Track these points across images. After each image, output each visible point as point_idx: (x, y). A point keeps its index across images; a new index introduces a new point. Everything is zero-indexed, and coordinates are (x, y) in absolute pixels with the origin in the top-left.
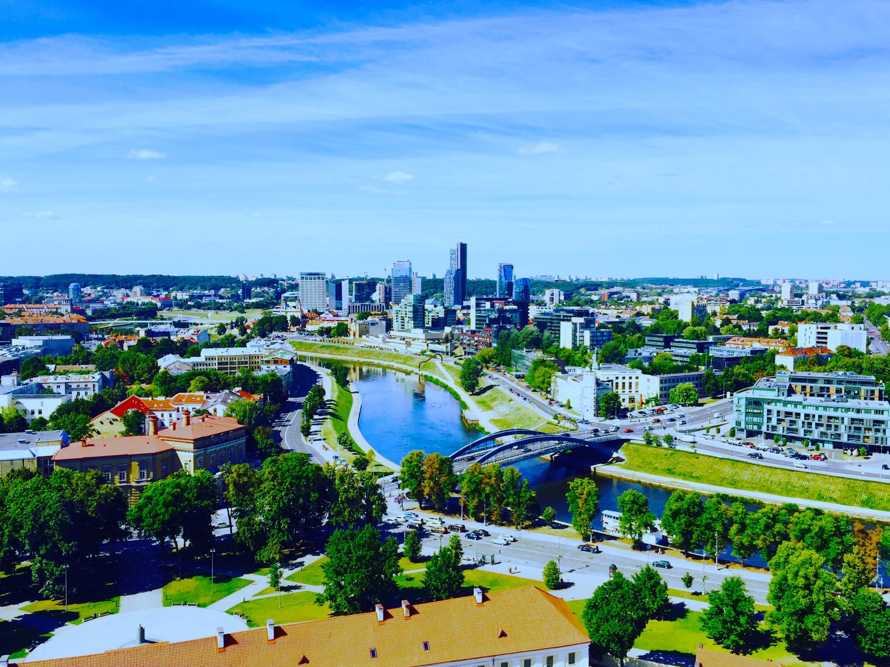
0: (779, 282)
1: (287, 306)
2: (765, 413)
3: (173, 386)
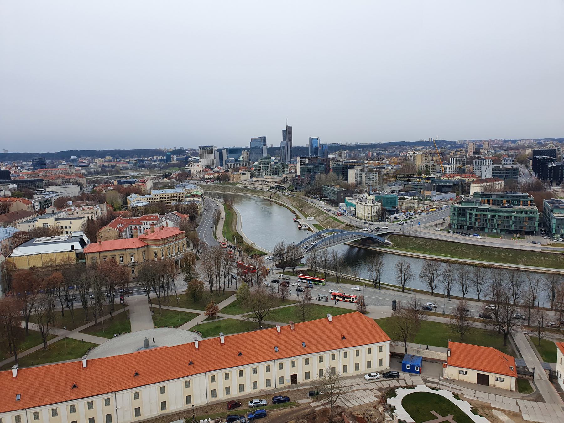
2: (468, 215)
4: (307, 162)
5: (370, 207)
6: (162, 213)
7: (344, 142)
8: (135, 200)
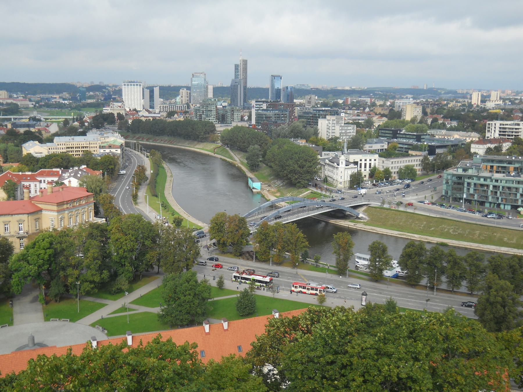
2: (466, 185)
3: (35, 164)
4: (265, 108)
5: (343, 170)
6: (66, 168)
7: (312, 85)
8: (34, 149)
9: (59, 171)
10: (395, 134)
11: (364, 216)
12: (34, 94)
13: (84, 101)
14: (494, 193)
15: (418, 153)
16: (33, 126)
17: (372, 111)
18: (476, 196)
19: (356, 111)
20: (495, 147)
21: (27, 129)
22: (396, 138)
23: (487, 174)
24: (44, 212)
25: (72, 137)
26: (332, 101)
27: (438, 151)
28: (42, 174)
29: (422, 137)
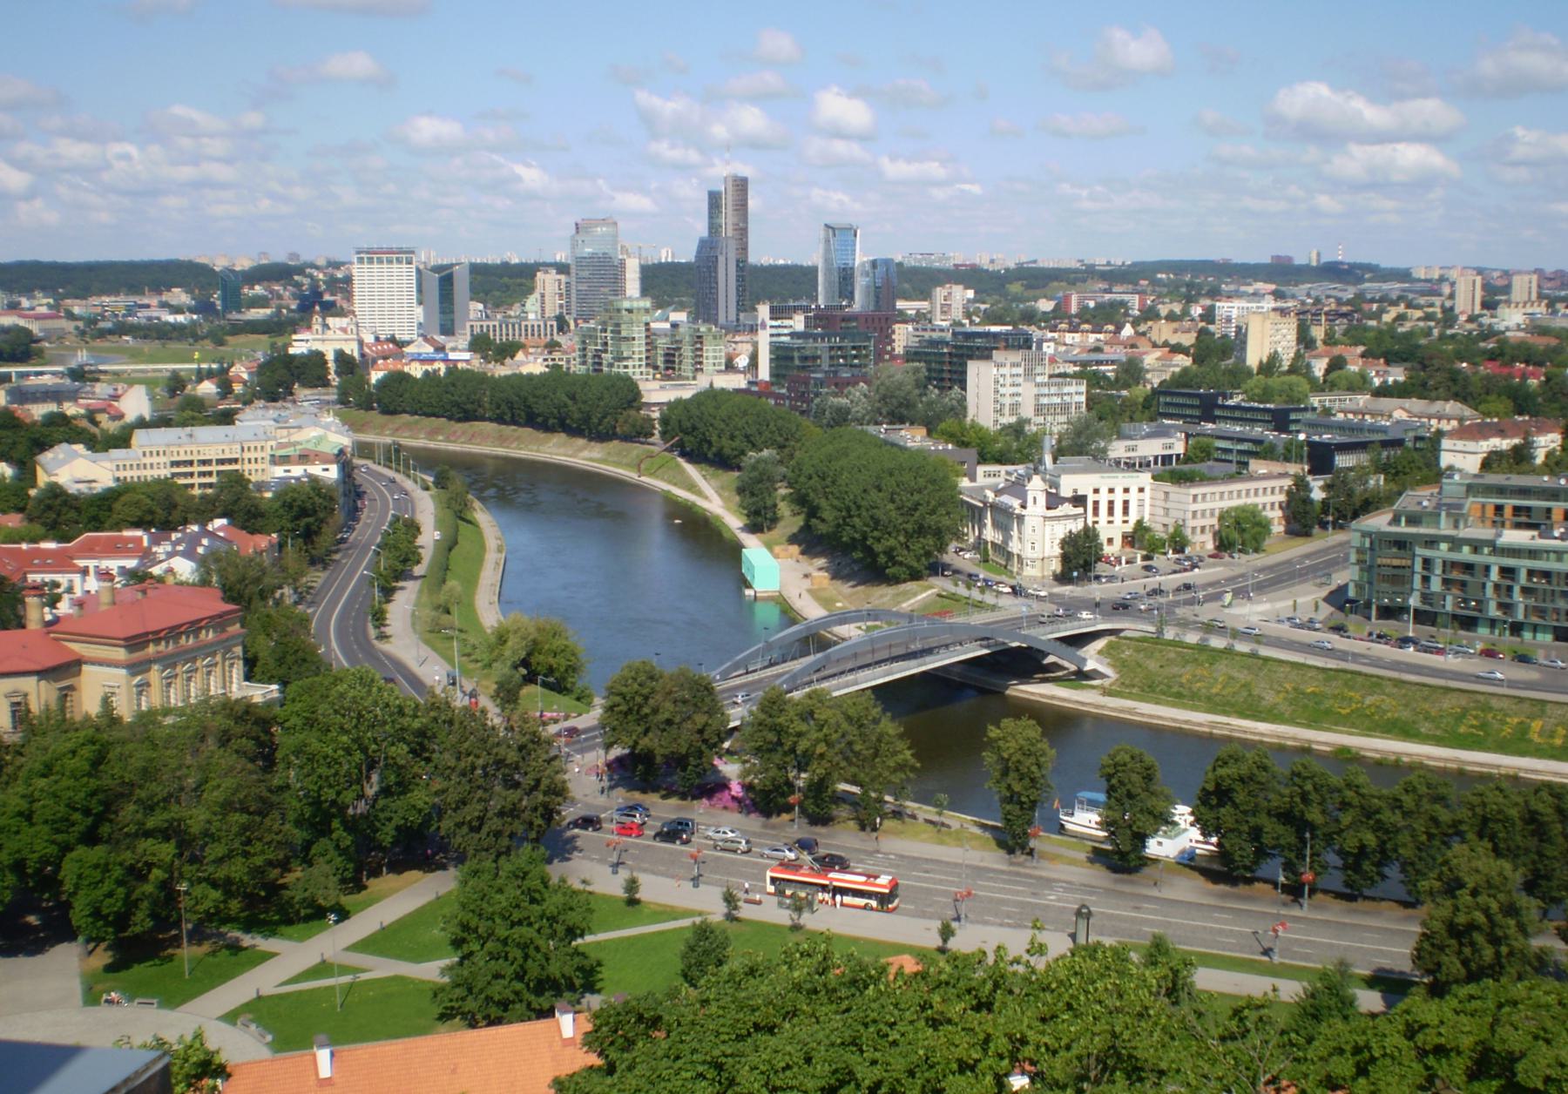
0: (1453, 275)
1: (326, 326)
2: (1418, 567)
6: (167, 526)
9: (140, 539)
10: (1208, 409)
11: (1101, 668)
12: (83, 294)
13: (234, 316)
14: (1503, 591)
15: (1277, 467)
16: (73, 396)
17: (1144, 334)
18: (1449, 599)
19: (1092, 337)
20: (1515, 449)
21: (52, 407)
22: (1213, 420)
23: (1486, 533)
24: (85, 668)
25: (188, 429)
26: (1016, 303)
27: (1342, 461)
28: (89, 551)
29: (1293, 416)
